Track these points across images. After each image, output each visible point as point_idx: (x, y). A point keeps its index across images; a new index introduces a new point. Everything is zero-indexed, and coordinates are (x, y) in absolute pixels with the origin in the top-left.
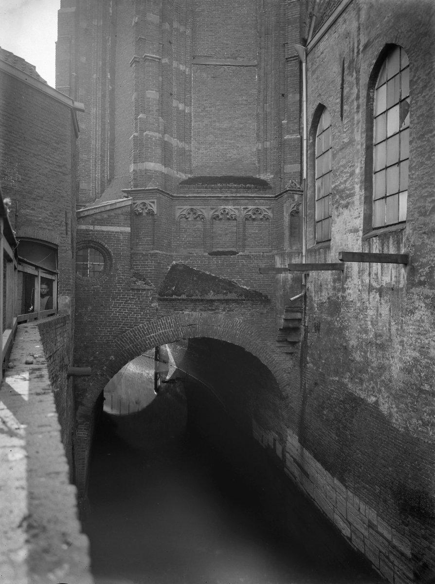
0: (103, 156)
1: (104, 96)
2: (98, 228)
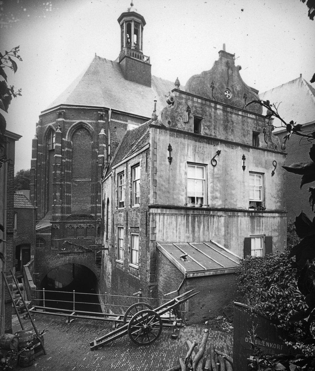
0: (45, 205)
1: (45, 186)
2: (42, 234)
